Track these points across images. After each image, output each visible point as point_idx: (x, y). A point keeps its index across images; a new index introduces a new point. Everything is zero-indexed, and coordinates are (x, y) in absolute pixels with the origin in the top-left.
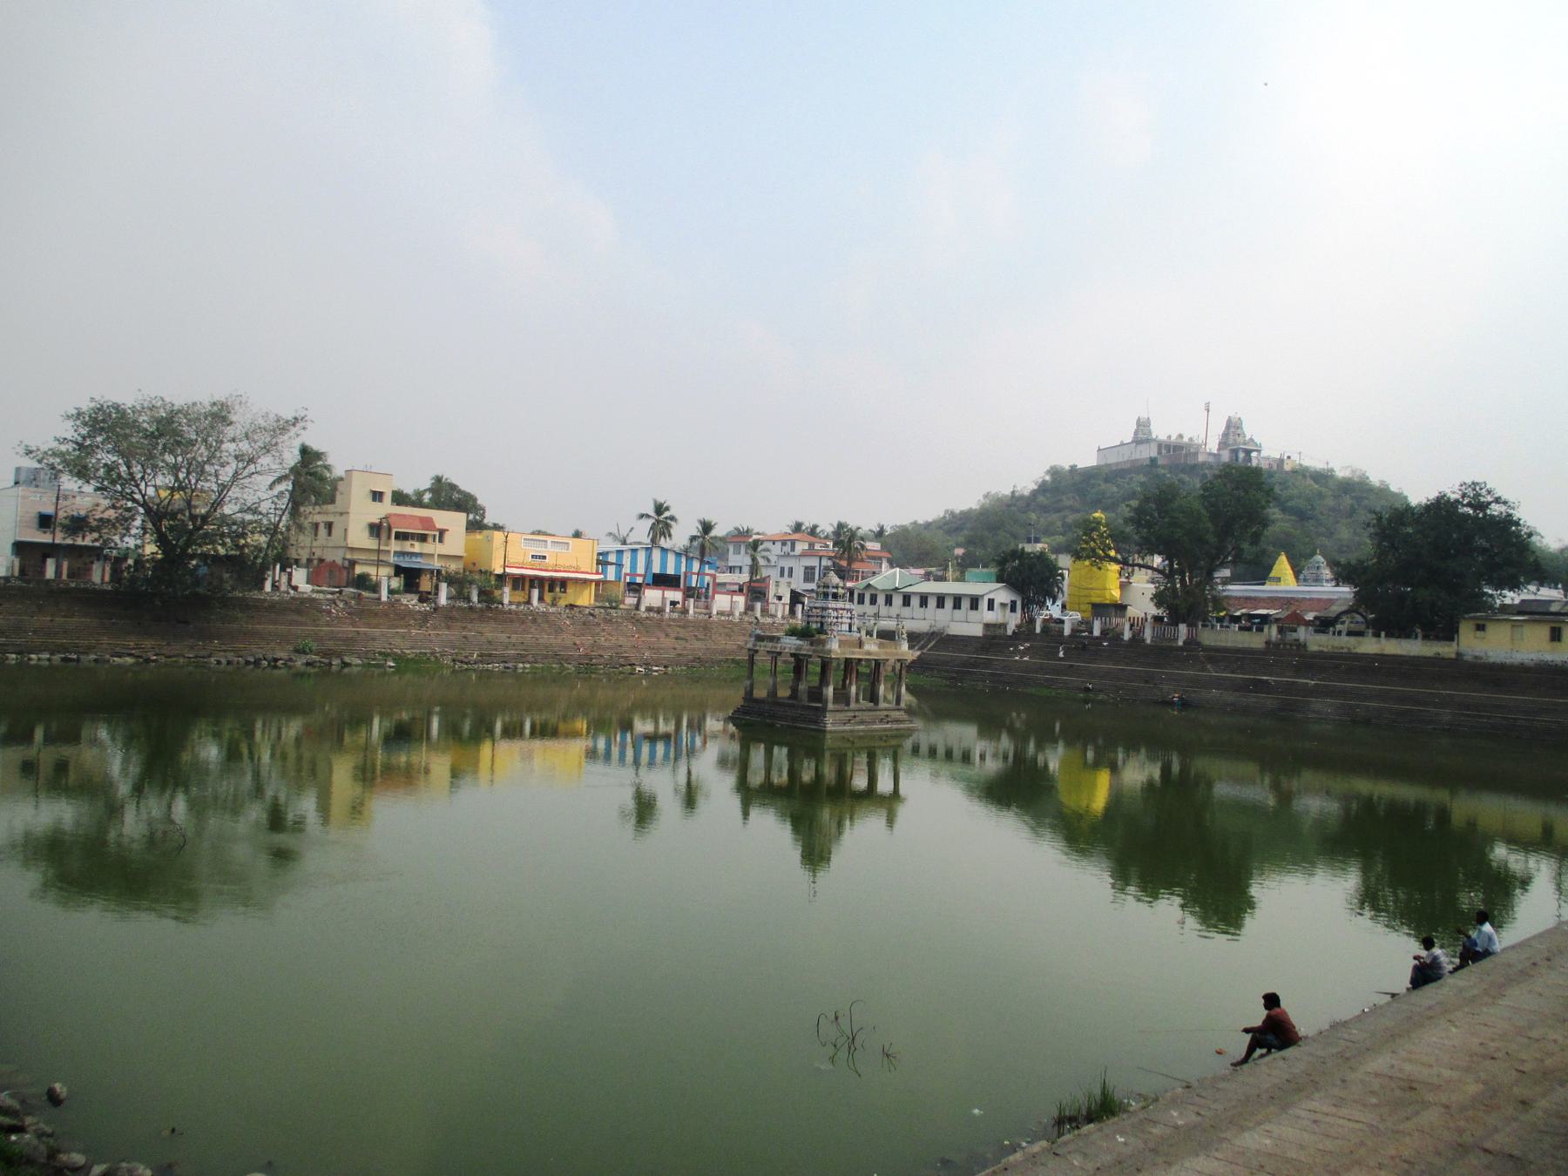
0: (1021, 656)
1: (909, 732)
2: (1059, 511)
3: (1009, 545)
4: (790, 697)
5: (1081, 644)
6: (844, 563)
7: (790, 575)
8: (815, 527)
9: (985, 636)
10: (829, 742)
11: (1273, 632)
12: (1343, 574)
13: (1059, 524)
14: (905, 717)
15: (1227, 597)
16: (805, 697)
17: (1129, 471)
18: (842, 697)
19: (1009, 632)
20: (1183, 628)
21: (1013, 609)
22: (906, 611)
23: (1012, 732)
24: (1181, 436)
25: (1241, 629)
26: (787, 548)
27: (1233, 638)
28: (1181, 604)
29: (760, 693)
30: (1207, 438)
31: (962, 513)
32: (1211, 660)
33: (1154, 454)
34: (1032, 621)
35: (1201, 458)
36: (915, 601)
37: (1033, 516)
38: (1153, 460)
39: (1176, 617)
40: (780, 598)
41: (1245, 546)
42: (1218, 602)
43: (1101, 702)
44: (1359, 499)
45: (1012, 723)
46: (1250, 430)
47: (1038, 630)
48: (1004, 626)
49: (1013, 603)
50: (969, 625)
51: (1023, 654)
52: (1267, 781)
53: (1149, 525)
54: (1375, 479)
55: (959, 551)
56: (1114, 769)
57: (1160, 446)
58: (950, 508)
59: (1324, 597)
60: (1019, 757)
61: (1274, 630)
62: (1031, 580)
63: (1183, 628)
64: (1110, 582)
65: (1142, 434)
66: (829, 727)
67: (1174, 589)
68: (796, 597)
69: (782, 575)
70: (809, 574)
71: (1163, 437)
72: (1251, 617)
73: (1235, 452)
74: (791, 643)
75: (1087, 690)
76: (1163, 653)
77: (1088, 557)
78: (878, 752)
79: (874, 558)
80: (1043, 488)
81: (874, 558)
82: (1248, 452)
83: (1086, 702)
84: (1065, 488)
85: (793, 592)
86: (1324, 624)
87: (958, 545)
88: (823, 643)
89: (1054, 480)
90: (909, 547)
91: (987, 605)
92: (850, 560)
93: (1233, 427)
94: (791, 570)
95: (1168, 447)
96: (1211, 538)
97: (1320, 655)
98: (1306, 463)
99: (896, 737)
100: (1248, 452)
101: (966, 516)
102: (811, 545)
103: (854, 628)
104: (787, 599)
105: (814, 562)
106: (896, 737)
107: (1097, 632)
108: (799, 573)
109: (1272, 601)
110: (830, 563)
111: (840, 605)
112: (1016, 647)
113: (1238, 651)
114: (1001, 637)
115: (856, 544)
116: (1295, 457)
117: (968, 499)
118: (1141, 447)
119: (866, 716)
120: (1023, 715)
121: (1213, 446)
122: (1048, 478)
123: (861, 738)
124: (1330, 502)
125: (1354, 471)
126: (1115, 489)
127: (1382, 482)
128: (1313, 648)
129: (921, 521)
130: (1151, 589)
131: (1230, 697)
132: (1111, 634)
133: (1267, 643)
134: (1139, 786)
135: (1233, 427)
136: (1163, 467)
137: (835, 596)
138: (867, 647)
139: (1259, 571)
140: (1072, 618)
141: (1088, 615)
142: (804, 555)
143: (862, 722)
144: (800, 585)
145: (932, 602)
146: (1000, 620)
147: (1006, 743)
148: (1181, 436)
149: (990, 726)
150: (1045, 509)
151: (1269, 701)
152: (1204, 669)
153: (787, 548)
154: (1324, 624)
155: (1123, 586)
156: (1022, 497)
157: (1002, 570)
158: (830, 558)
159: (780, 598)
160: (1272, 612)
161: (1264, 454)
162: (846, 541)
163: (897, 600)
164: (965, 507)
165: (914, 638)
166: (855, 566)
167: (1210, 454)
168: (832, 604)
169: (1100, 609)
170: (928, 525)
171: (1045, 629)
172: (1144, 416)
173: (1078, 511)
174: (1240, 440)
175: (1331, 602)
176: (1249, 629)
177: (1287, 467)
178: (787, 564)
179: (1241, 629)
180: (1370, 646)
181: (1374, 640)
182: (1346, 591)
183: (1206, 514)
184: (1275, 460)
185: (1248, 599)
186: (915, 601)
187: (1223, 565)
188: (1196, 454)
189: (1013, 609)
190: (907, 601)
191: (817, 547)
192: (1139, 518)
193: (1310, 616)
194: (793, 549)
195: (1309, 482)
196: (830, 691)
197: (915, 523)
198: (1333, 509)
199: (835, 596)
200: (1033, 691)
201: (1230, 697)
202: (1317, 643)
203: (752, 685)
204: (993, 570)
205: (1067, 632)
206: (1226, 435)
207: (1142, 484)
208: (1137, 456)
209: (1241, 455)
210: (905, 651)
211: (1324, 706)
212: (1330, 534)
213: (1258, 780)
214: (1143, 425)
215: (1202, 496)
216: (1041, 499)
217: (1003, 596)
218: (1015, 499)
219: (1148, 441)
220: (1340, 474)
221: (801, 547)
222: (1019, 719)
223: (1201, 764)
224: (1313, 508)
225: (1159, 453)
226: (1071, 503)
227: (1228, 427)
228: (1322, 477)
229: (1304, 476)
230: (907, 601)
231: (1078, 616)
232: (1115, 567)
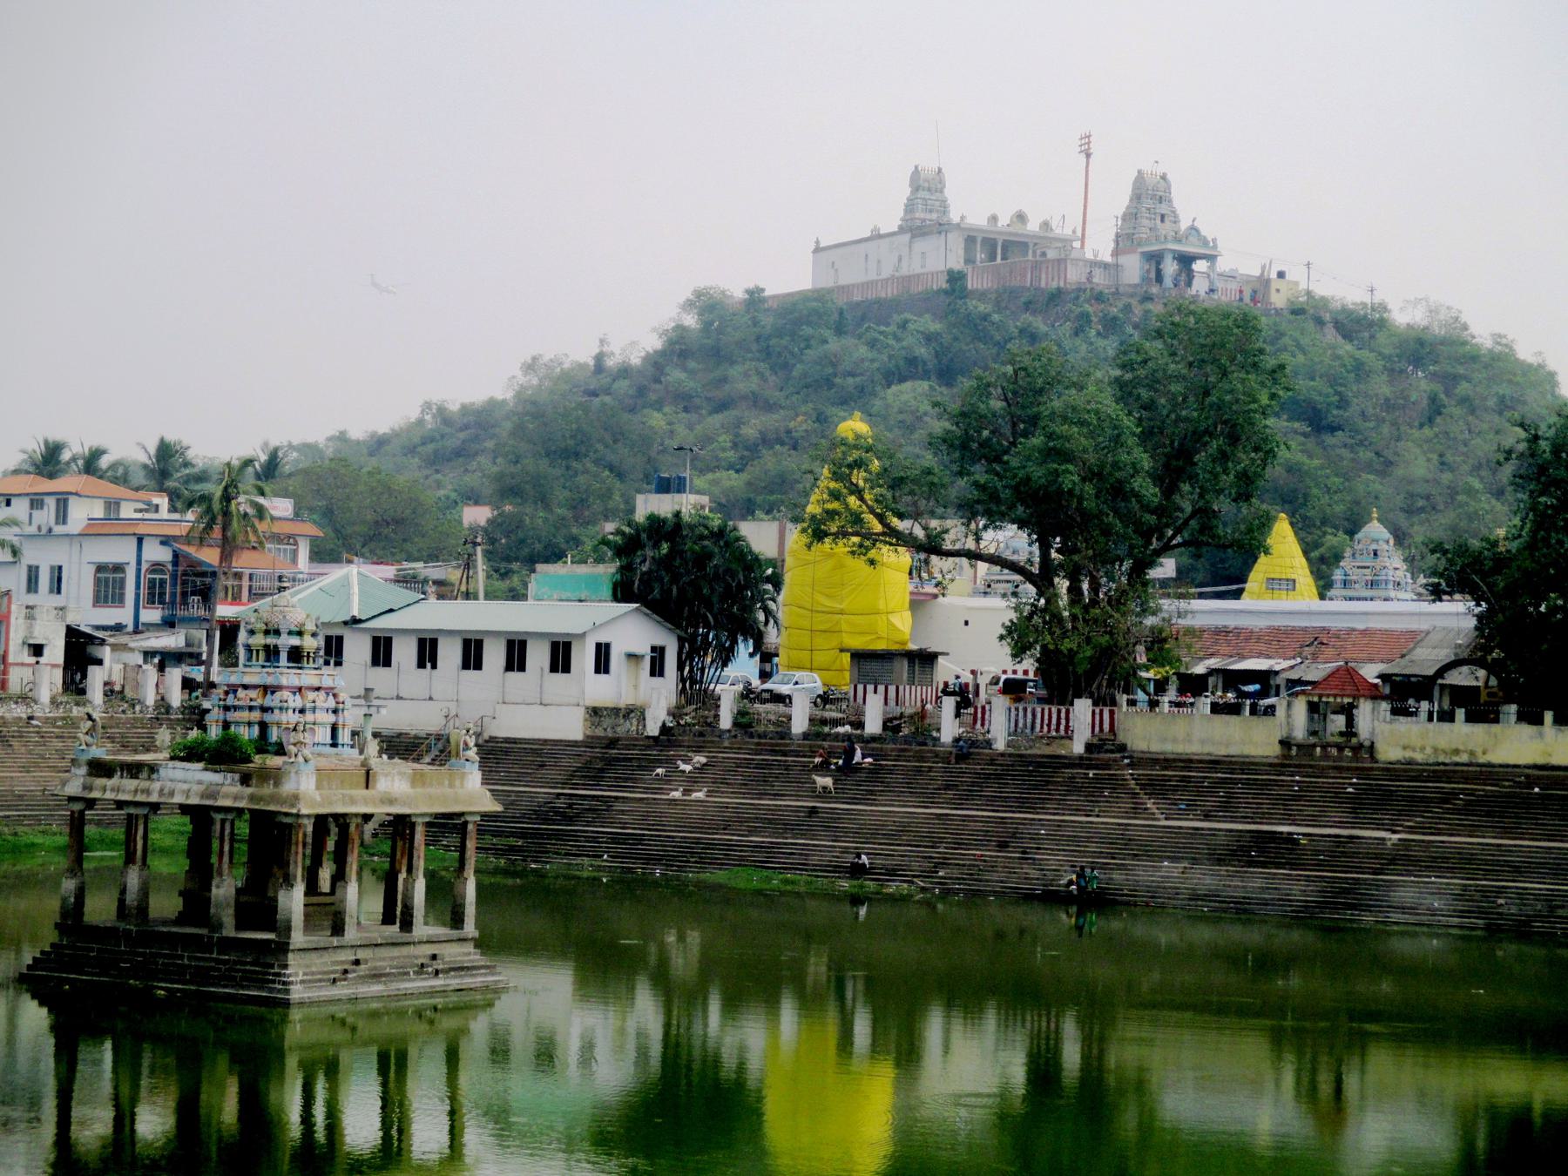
0: (687, 792)
1: (490, 996)
2: (722, 406)
3: (644, 498)
4: (181, 920)
7: (57, 585)
8: (96, 454)
10: (297, 1031)
11: (1294, 718)
12: (1456, 571)
13: (725, 439)
16: (228, 919)
17: (893, 305)
19: (653, 729)
20: (1082, 709)
21: (657, 669)
23: (663, 982)
24: (1021, 217)
25: (1216, 709)
26: (46, 516)
27: (1198, 732)
28: (1073, 658)
29: (100, 909)
30: (1087, 227)
31: (465, 409)
32: (1155, 788)
33: (956, 262)
34: (711, 701)
35: (1074, 276)
36: (404, 652)
37: (657, 420)
38: (955, 278)
40: (37, 650)
41: (1222, 505)
43: (896, 899)
46: (1194, 208)
47: (726, 722)
48: (635, 712)
49: (658, 653)
50: (552, 711)
51: (692, 781)
52: (1289, 1079)
53: (992, 455)
54: (1482, 331)
55: (477, 515)
57: (970, 241)
58: (436, 398)
60: (673, 1047)
62: (699, 589)
63: (1082, 709)
64: (879, 594)
66: (297, 993)
69: (32, 584)
70: (108, 584)
72: (1233, 679)
73: (1155, 258)
74: (187, 782)
75: (857, 871)
76: (1036, 774)
78: (344, 1057)
79: (277, 538)
80: (678, 348)
81: (277, 538)
82: (1186, 261)
83: (856, 900)
84: (747, 352)
85: (72, 633)
86: (1404, 692)
87: (474, 499)
88: (275, 776)
89: (707, 325)
90: (362, 508)
91: (595, 664)
92: (228, 548)
93: (1150, 197)
95: (990, 245)
96: (1150, 491)
97: (1406, 771)
98: (1321, 290)
100: (1186, 261)
101: (479, 421)
102: (112, 505)
103: (344, 736)
104: (56, 652)
105: (120, 552)
107: (873, 726)
108: (80, 583)
109: (1277, 639)
111: (308, 677)
112: (670, 762)
113: (1214, 764)
116: (1296, 274)
117: (484, 375)
118: (921, 245)
119: (384, 959)
121: (1100, 245)
122: (691, 321)
123: (374, 1015)
124: (1381, 387)
125: (1433, 311)
126: (863, 351)
127: (1498, 338)
128: (1389, 752)
129: (357, 433)
130: (999, 611)
131: (1206, 878)
132: (908, 732)
133: (1285, 743)
134: (982, 1115)
135: (1150, 197)
136: (982, 296)
137: (296, 655)
138: (382, 785)
139: (1226, 567)
140: (801, 690)
141: (844, 682)
142: (93, 532)
143: (376, 976)
146: (625, 700)
148: (1021, 217)
149: (604, 966)
151: (1296, 887)
152: (1138, 810)
153: (46, 516)
154: (1404, 692)
155: (918, 604)
156: (625, 371)
157: (626, 569)
158: (165, 541)
159: (37, 650)
161: (1223, 265)
163: (357, 649)
165: (498, 755)
166: (244, 561)
167: (1094, 264)
168: (288, 676)
169: (871, 663)
170: (379, 444)
171: (743, 722)
172: (929, 164)
173: (770, 407)
174: (1166, 229)
176: (1234, 709)
177: (1278, 300)
178: (43, 557)
179: (1216, 709)
180: (1517, 744)
181: (1527, 730)
182: (1457, 616)
184: (1248, 279)
185: (1221, 632)
186: (404, 652)
188: (1061, 262)
189: (657, 669)
190: (382, 652)
191: (127, 511)
192: (969, 443)
193: (1370, 672)
194: (62, 517)
195: (1331, 335)
196: (293, 901)
197: (342, 437)
198: (1388, 405)
199: (296, 655)
200: (719, 876)
201: (1206, 878)
202: (1397, 738)
203: (80, 894)
204: (607, 571)
205: (799, 725)
206: (1131, 216)
207: (929, 338)
208: (912, 266)
209: (1170, 268)
210: (469, 791)
212: (1385, 466)
214: (926, 189)
216: (675, 375)
217: (634, 632)
218: (601, 377)
222: (684, 948)
224: (1343, 403)
225: (969, 260)
226: (754, 384)
227: (1137, 197)
228: (1358, 325)
229: (1320, 322)
230: (382, 652)
231: (814, 683)
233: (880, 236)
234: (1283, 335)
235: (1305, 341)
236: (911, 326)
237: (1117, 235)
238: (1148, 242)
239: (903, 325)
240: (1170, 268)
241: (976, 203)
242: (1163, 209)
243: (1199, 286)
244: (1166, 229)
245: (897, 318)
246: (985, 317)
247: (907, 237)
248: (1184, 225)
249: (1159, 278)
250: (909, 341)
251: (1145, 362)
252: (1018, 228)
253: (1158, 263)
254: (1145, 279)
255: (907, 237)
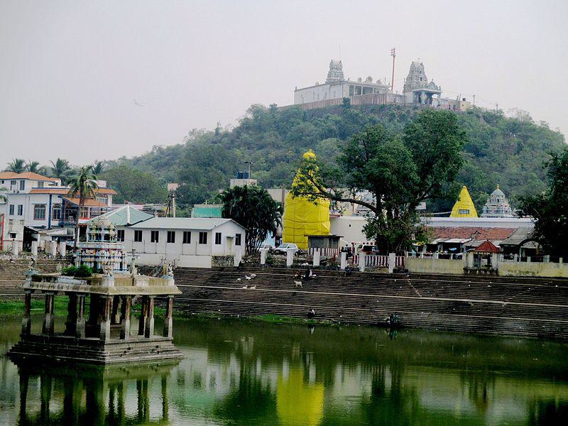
0: (249, 287)
2: (261, 147)
3: (233, 180)
5: (301, 269)
6: (76, 201)
8: (35, 164)
9: (213, 269)
10: (107, 373)
11: (469, 260)
12: (527, 207)
14: (173, 347)
15: (431, 229)
16: (83, 333)
17: (324, 110)
18: (119, 332)
19: (236, 264)
20: (392, 256)
21: (238, 242)
22: (138, 245)
24: (370, 79)
25: (441, 257)
26: (17, 187)
28: (389, 238)
29: (36, 329)
30: (392, 81)
33: (346, 95)
35: (389, 100)
36: (146, 236)
37: (238, 152)
38: (346, 101)
39: (384, 246)
40: (14, 235)
41: (443, 183)
42: (420, 234)
44: (525, 138)
45: (240, 348)
46: (431, 75)
47: (263, 262)
49: (239, 236)
50: (200, 258)
51: (251, 283)
52: (467, 391)
53: (359, 165)
54: (537, 120)
55: (173, 187)
56: (329, 382)
57: (351, 87)
59: (508, 227)
61: (471, 256)
62: (254, 213)
63: (392, 256)
64: (320, 216)
65: (335, 78)
66: (108, 360)
67: (381, 221)
68: (29, 236)
69: (12, 212)
71: (354, 79)
73: (418, 94)
75: (310, 316)
76: (376, 280)
77: (305, 193)
78: (125, 383)
79: (100, 195)
80: (245, 126)
82: (430, 94)
83: (310, 326)
84: (270, 127)
85: (26, 229)
86: (509, 251)
88: (99, 281)
90: (132, 184)
91: (215, 240)
93: (416, 72)
94: (21, 208)
95: (359, 89)
96: (417, 178)
98: (478, 105)
99: (166, 365)
100: (430, 94)
101: (173, 153)
102: (41, 183)
103: (125, 267)
104: (20, 236)
105: (44, 200)
106: (166, 365)
108: (29, 211)
109: (463, 231)
110: (60, 201)
111: (112, 245)
112: (243, 276)
113: (440, 277)
114: (229, 269)
115: (88, 183)
117: (175, 136)
118: (333, 89)
120: (251, 339)
121: (398, 89)
122: (250, 116)
123: (136, 368)
124: (500, 140)
125: (519, 113)
126: (313, 127)
129: (129, 157)
131: (436, 318)
132: (330, 265)
133: (466, 269)
135: (416, 72)
136: (356, 107)
137: (107, 237)
138: (138, 284)
139: (444, 205)
140: (290, 251)
141: (306, 247)
142: (34, 193)
143: (136, 354)
144: (32, 223)
145: (163, 237)
147: (234, 366)
148: (370, 79)
149: (219, 350)
150: (248, 146)
151: (469, 321)
152: (412, 294)
153: (17, 187)
154: (509, 251)
156: (226, 134)
159: (14, 235)
160: (463, 241)
161: (443, 96)
162: (78, 183)
164: (173, 144)
165: (180, 273)
166: (88, 203)
169: (315, 240)
170: (137, 161)
172: (336, 60)
173: (279, 147)
175: (512, 231)
176: (447, 257)
177: (463, 109)
178: (16, 202)
179: (441, 257)
181: (553, 264)
182: (528, 223)
183: (409, 159)
185: (442, 229)
186: (146, 236)
187: (423, 199)
189: (238, 242)
190: (138, 236)
191: (46, 185)
193: (496, 244)
194: (22, 187)
195: (482, 121)
198: (503, 147)
199: (107, 237)
200: (261, 317)
201: (436, 318)
202: (506, 267)
204: (220, 206)
206: (410, 78)
209: (424, 97)
210: (170, 286)
211: (516, 325)
212: (502, 169)
213: (460, 390)
214: (335, 68)
215: (405, 138)
216: (245, 136)
217: (230, 229)
219: (341, 83)
220: (509, 115)
221: (29, 186)
222: (248, 343)
223: (410, 380)
224: (487, 146)
226: (273, 139)
227: (412, 71)
229: (478, 117)
230: (138, 236)
232: (328, 202)
233: (319, 86)
234: (464, 121)
235: (473, 124)
236: (330, 118)
237: (405, 85)
238: (416, 88)
239: (327, 118)
240: (424, 97)
241: (353, 74)
242: (421, 76)
243: (435, 104)
244: (423, 83)
245: (325, 115)
246: (357, 115)
247: (329, 86)
248: (429, 81)
249: (420, 101)
250: (329, 123)
251: (415, 131)
252: (369, 83)
253: (420, 95)
254: (415, 101)
255: (329, 86)
